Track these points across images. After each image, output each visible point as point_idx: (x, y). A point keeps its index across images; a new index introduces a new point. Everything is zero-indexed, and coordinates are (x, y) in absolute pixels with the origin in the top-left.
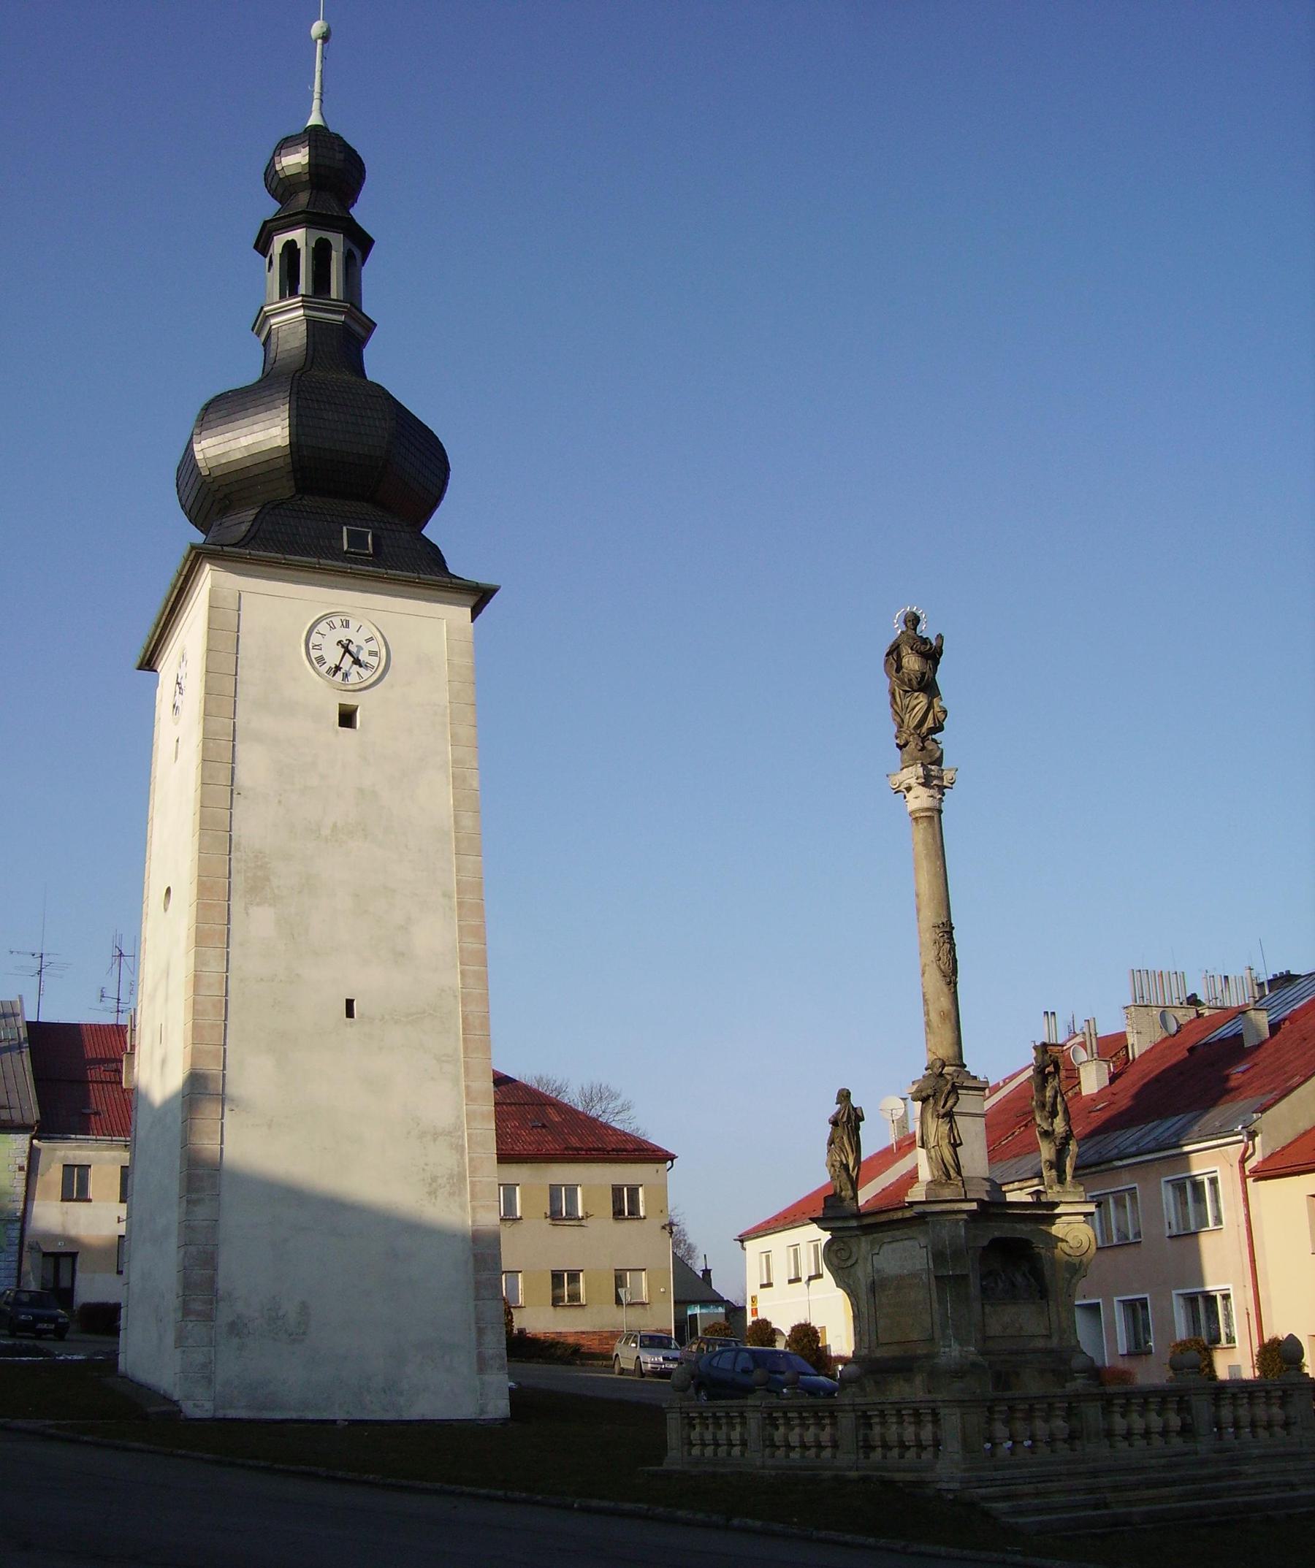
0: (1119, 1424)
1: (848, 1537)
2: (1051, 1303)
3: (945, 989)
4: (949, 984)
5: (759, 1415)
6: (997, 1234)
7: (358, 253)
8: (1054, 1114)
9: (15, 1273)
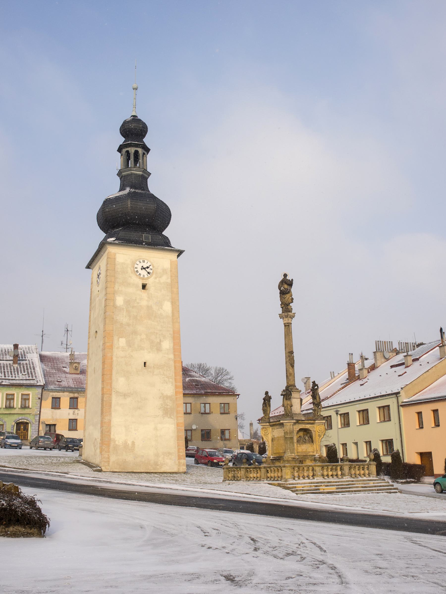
6: (301, 427)
7: (146, 153)
9: (37, 430)
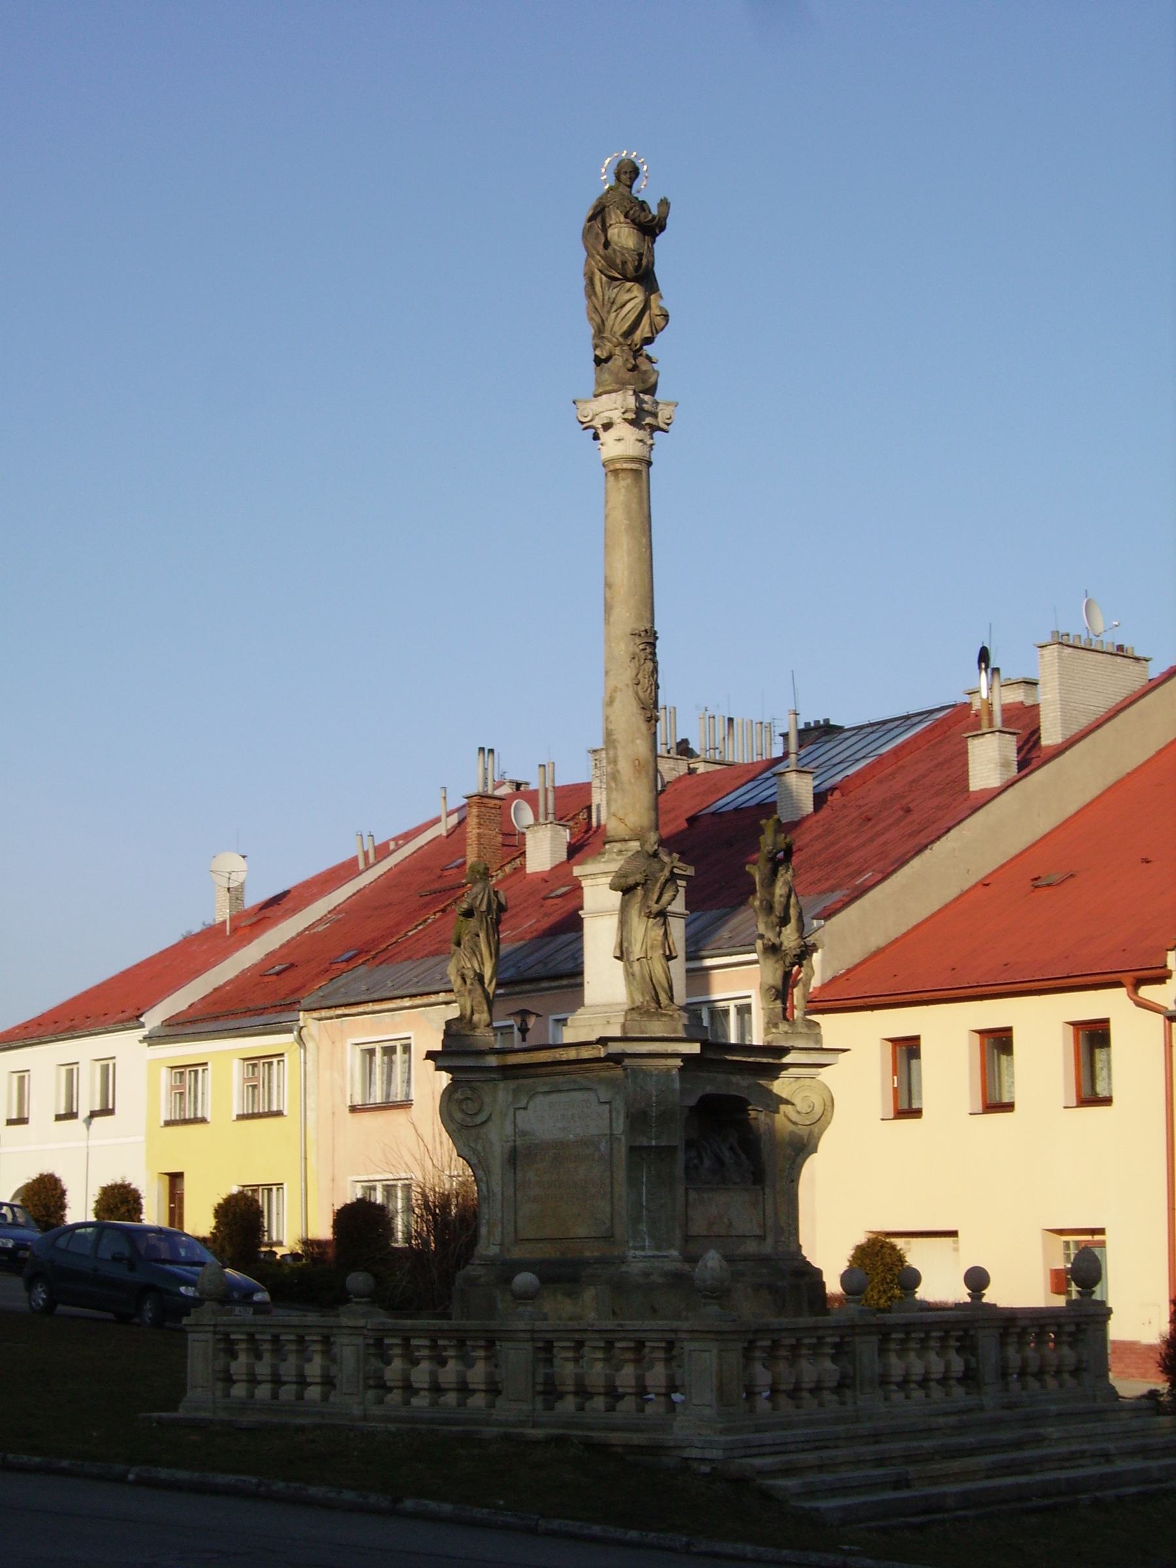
0: (897, 1366)
1: (596, 1529)
2: (767, 1190)
3: (643, 727)
4: (649, 720)
5: (359, 1340)
6: (709, 1089)
8: (784, 921)
